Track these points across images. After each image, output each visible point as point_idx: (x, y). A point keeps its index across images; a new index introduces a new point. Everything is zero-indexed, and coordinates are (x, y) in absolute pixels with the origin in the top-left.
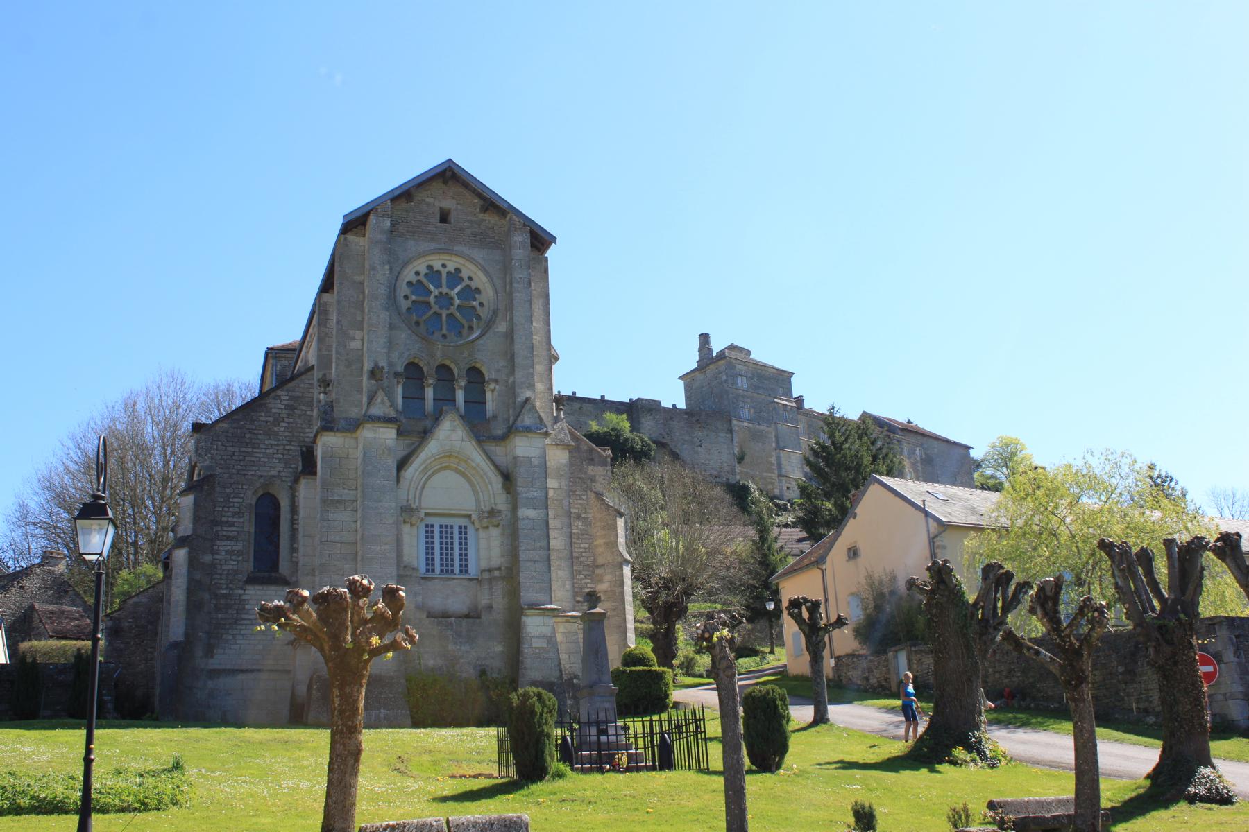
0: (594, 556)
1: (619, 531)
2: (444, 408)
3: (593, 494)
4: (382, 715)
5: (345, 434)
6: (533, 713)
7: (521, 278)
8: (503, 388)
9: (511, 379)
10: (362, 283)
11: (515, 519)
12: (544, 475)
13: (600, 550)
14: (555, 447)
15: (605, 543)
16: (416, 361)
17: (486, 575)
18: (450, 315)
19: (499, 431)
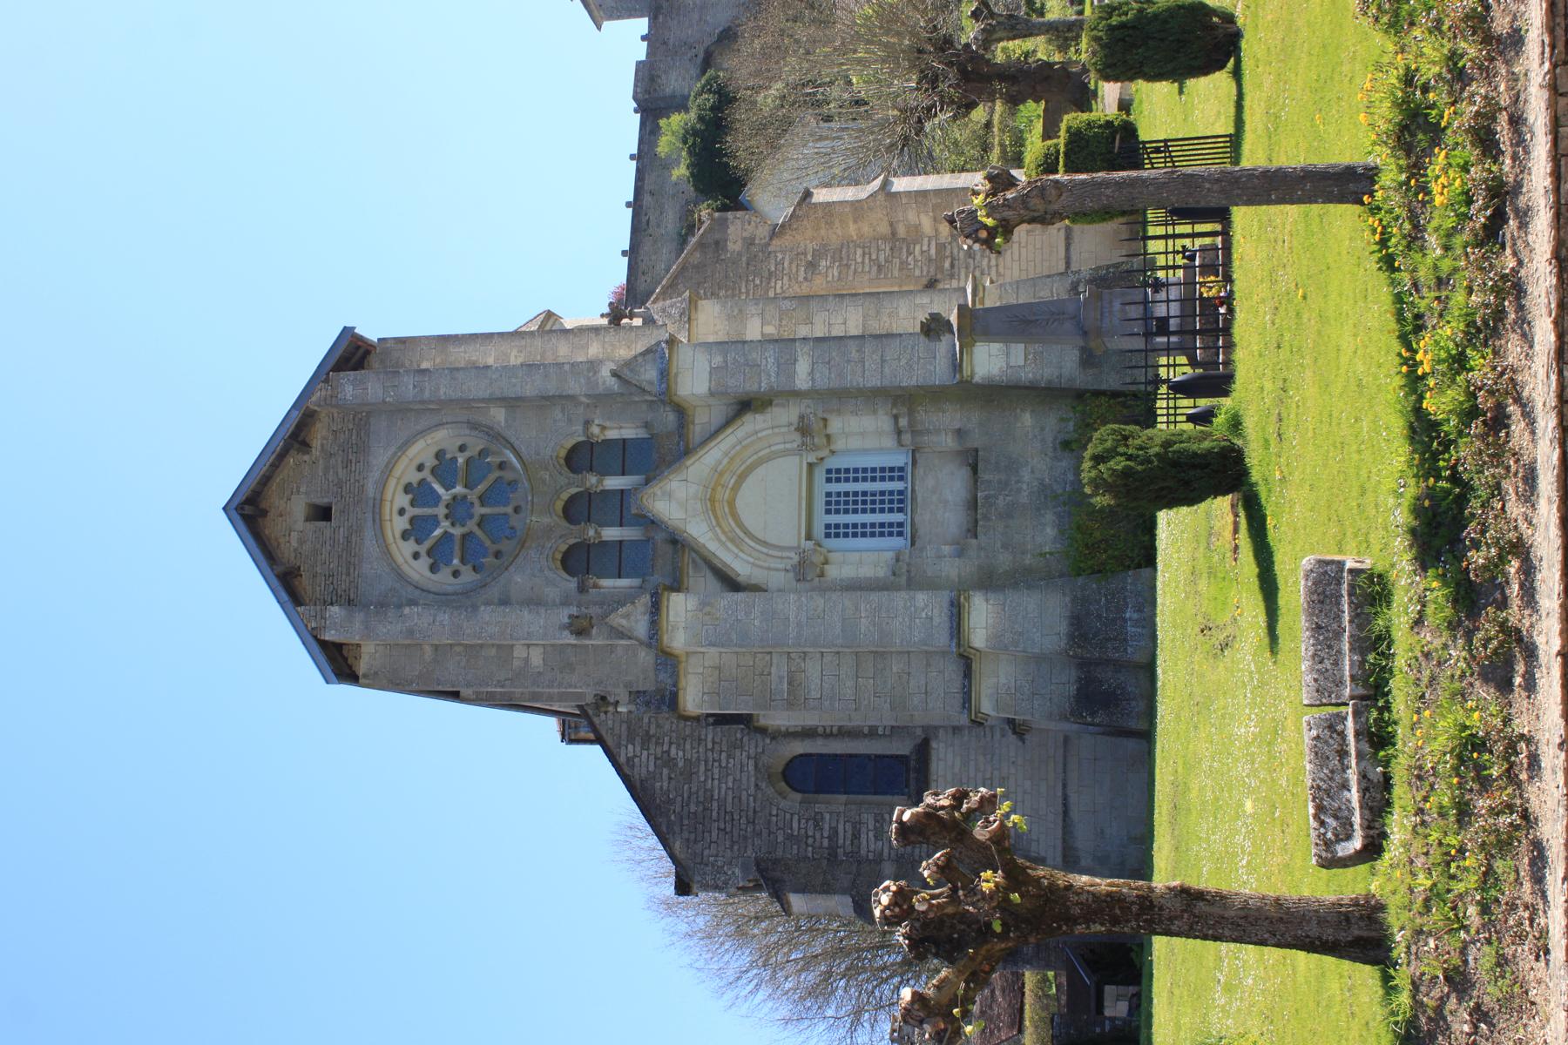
0: (876, 239)
1: (835, 199)
2: (634, 511)
3: (774, 242)
4: (1135, 616)
5: (682, 673)
6: (1127, 473)
7: (414, 386)
8: (598, 411)
9: (583, 399)
10: (436, 648)
11: (812, 394)
12: (740, 345)
13: (866, 229)
14: (694, 323)
15: (855, 221)
16: (559, 556)
17: (907, 438)
18: (483, 500)
19: (671, 417)
